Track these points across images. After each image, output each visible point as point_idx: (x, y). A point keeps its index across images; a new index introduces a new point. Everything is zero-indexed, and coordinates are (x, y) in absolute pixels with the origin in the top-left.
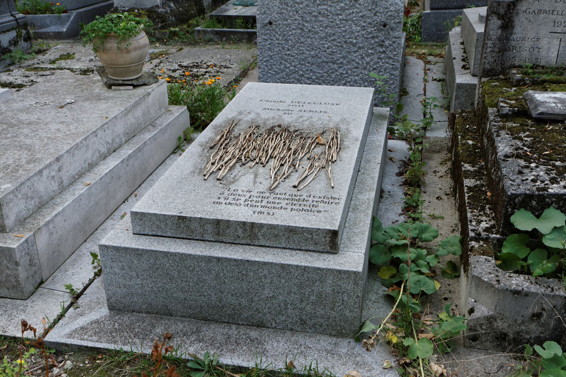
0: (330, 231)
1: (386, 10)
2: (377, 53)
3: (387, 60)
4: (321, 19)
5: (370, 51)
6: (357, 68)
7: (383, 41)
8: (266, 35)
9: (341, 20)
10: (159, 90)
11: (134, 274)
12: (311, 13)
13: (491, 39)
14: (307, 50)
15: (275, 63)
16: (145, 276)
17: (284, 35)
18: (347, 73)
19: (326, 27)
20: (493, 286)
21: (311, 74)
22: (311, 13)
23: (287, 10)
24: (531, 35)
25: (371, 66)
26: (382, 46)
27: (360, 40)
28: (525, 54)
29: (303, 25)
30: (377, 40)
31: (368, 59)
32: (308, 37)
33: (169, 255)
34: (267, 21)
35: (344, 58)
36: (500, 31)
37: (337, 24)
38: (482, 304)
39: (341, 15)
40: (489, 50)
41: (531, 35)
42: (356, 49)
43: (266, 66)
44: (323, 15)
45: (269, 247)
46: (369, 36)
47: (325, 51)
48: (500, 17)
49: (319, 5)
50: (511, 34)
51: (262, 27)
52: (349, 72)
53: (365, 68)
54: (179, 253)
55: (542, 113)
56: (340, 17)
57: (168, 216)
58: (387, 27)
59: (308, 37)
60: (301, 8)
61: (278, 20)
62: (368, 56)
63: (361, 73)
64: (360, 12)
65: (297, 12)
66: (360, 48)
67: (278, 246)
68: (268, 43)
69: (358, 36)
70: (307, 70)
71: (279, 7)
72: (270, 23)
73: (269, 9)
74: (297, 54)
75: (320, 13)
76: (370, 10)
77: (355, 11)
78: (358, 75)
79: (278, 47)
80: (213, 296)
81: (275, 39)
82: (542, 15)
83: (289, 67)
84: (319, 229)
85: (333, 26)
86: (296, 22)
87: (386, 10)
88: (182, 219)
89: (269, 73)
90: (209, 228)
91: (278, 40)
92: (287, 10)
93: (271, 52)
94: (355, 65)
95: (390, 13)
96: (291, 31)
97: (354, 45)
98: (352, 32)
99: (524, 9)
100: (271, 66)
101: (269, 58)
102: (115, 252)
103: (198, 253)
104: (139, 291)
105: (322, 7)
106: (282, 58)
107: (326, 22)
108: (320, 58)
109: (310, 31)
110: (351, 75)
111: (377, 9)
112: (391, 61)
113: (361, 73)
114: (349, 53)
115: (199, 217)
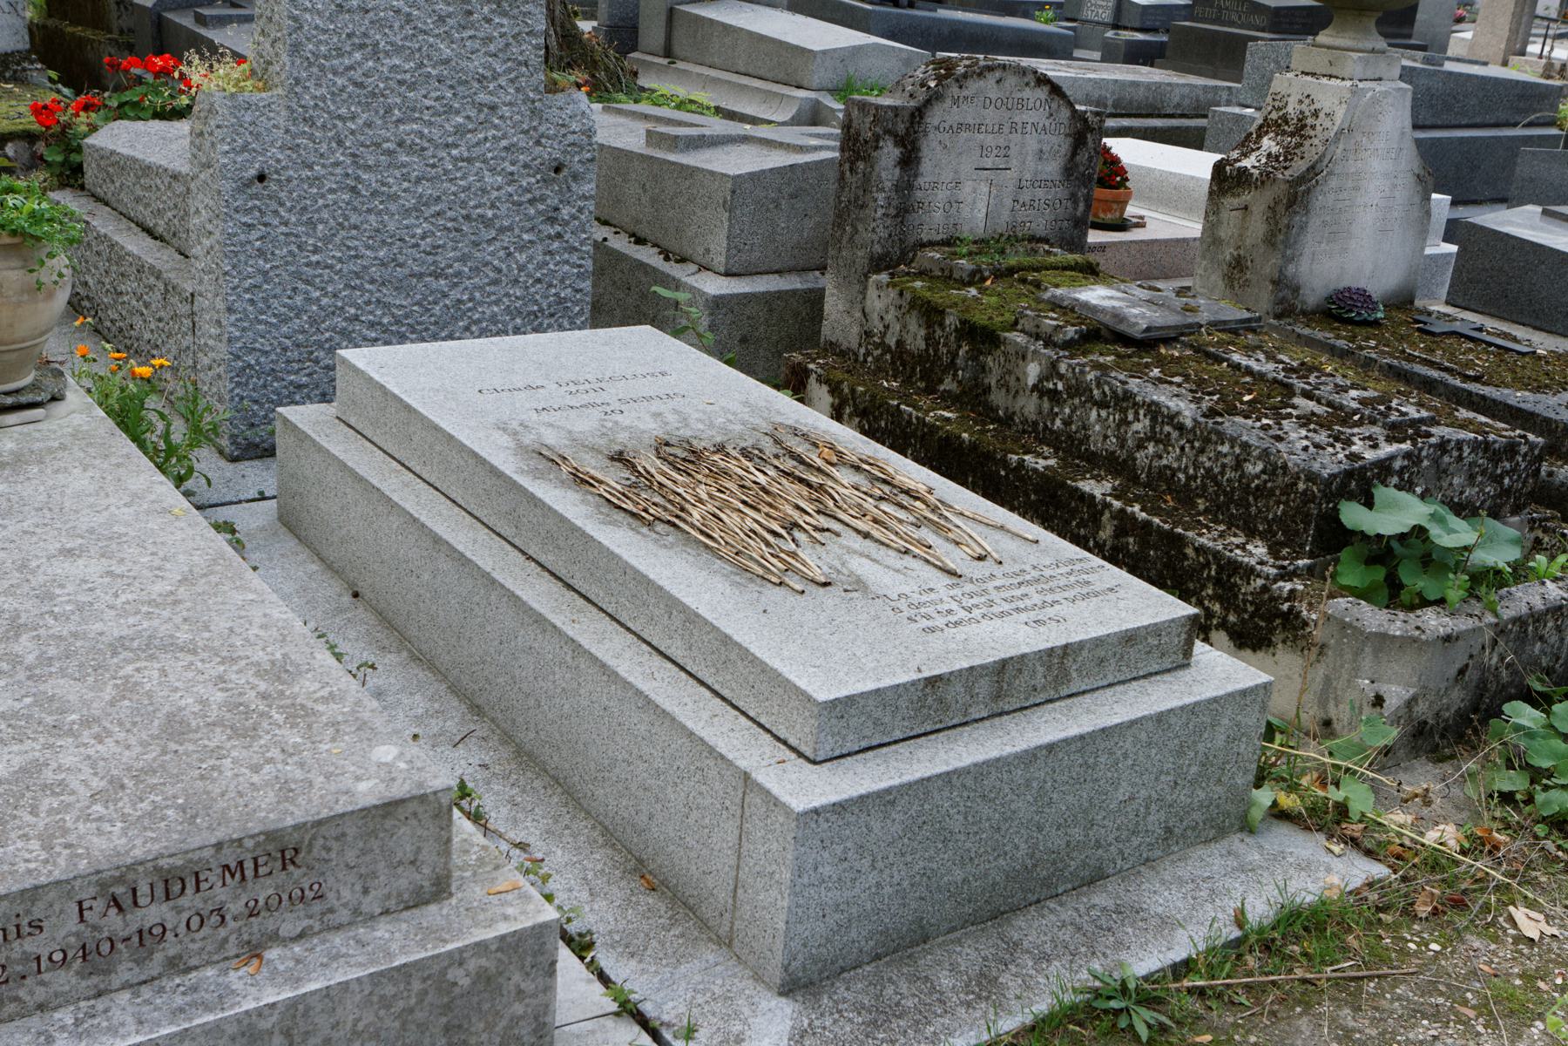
1: (563, 131)
3: (566, 256)
4: (404, 158)
5: (526, 237)
6: (495, 282)
7: (556, 209)
8: (248, 211)
9: (455, 159)
11: (866, 862)
12: (378, 145)
13: (883, 190)
14: (368, 247)
15: (278, 291)
18: (470, 300)
19: (418, 180)
20: (1415, 640)
24: (947, 176)
25: (529, 276)
26: (552, 220)
27: (504, 208)
28: (938, 215)
29: (358, 179)
30: (541, 207)
31: (522, 258)
32: (369, 211)
34: (253, 172)
35: (463, 259)
36: (897, 171)
37: (446, 172)
38: (1389, 681)
39: (457, 146)
40: (880, 212)
41: (947, 176)
42: (493, 233)
43: (252, 301)
44: (411, 149)
47: (414, 246)
48: (900, 141)
49: (399, 121)
50: (916, 176)
51: (239, 190)
52: (477, 295)
55: (1148, 329)
56: (454, 152)
58: (565, 172)
59: (369, 211)
60: (353, 132)
62: (521, 249)
64: (504, 137)
65: (340, 143)
66: (502, 230)
68: (254, 235)
69: (498, 198)
70: (368, 303)
71: (287, 131)
72: (261, 178)
73: (257, 136)
74: (340, 260)
76: (525, 132)
78: (497, 303)
79: (287, 244)
82: (964, 135)
83: (318, 299)
85: (437, 177)
86: (339, 171)
87: (563, 131)
88: (933, 682)
92: (312, 138)
93: (266, 261)
94: (492, 274)
95: (571, 138)
96: (323, 196)
97: (488, 223)
98: (484, 191)
99: (936, 123)
100: (265, 300)
101: (259, 279)
106: (297, 275)
107: (417, 166)
108: (401, 265)
109: (375, 194)
110: (481, 303)
111: (542, 129)
112: (574, 258)
113: (507, 295)
114: (476, 244)
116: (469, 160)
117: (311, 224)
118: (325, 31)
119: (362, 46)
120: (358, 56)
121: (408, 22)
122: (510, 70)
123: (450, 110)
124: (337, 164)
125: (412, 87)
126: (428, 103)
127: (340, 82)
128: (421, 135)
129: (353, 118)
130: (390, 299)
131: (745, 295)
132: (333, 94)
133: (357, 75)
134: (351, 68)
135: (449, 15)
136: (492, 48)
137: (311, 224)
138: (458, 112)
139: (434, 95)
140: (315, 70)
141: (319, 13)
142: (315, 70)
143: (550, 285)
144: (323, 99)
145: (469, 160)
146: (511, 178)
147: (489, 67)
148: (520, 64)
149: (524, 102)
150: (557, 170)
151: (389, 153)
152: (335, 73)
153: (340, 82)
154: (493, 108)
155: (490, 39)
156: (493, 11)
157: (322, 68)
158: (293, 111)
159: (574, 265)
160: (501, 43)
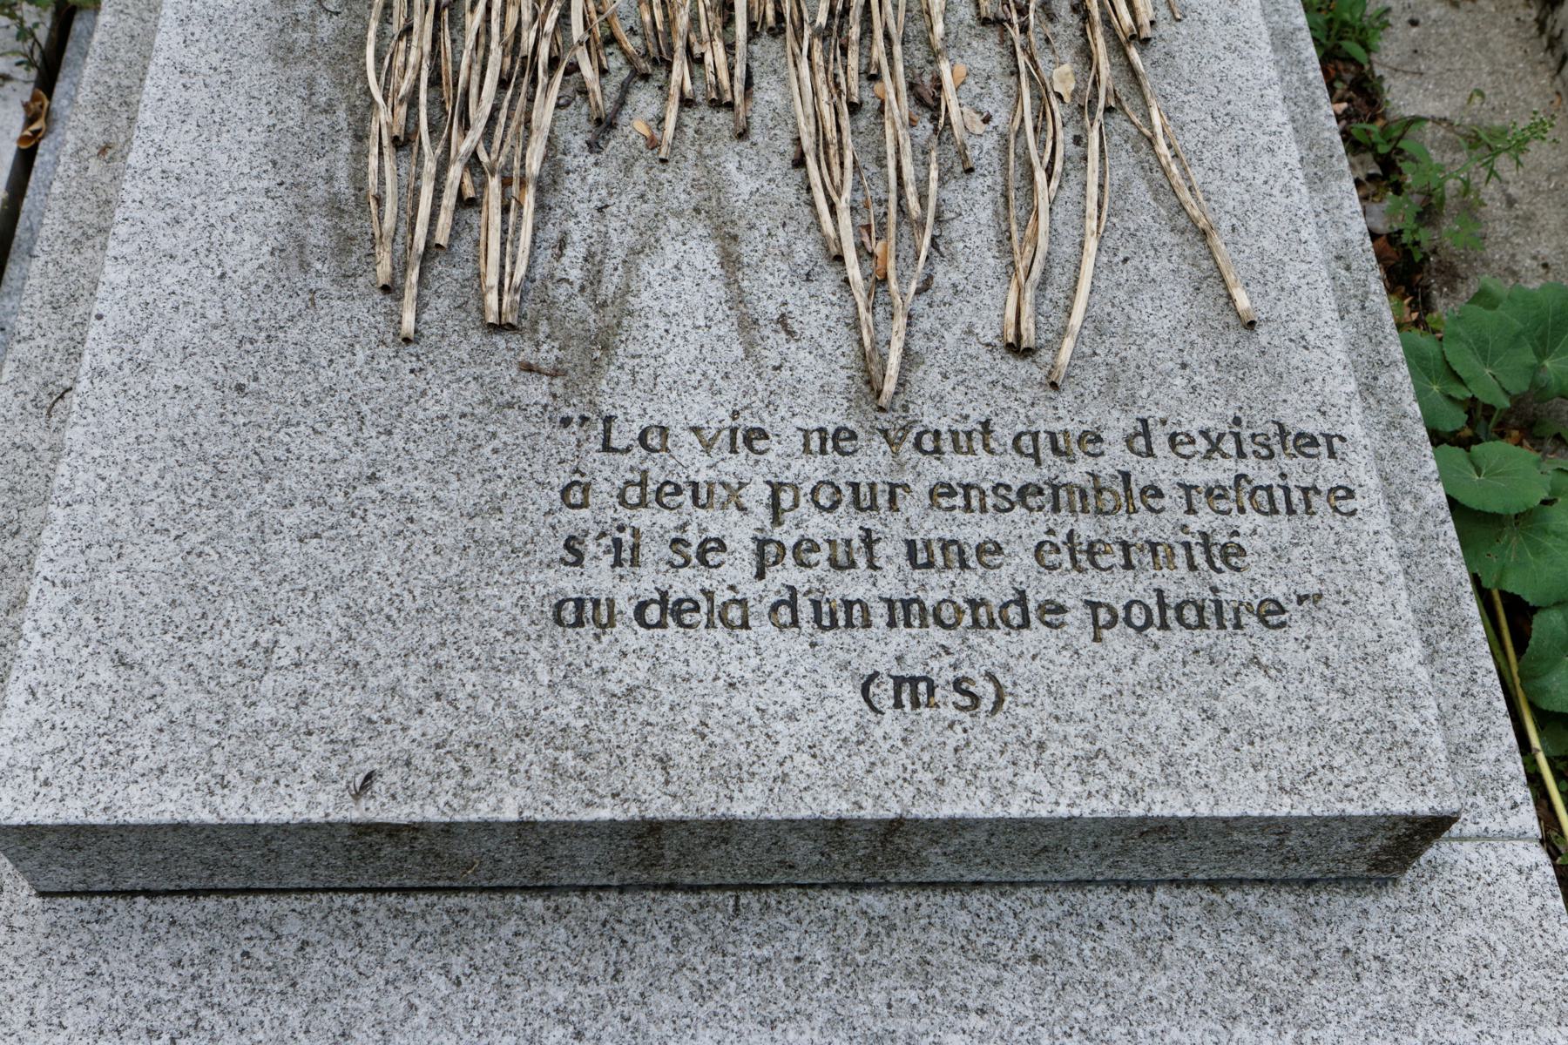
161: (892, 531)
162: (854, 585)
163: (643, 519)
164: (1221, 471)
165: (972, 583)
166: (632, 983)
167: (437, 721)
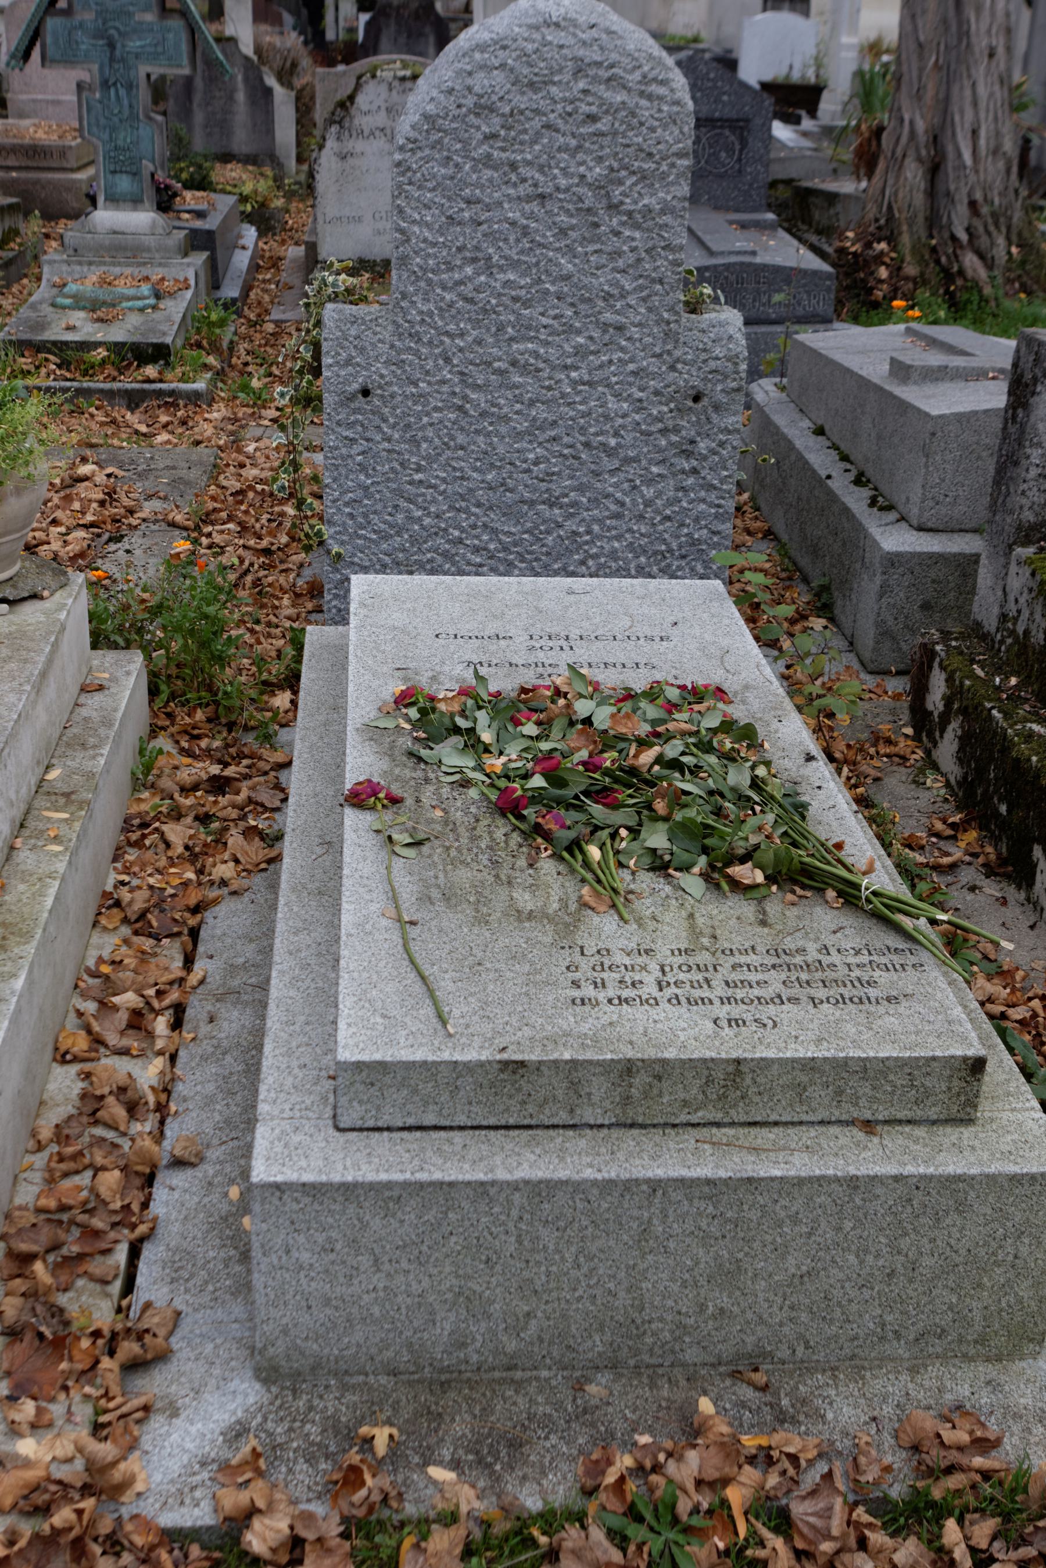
0: (965, 1059)
1: (704, 356)
2: (674, 475)
3: (703, 494)
4: (517, 379)
5: (655, 469)
6: (617, 516)
7: (692, 442)
8: (350, 425)
9: (574, 383)
10: (69, 605)
11: (365, 1261)
12: (489, 364)
14: (475, 469)
15: (379, 507)
16: (404, 1265)
17: (408, 426)
18: (588, 532)
19: (532, 403)
21: (485, 537)
22: (489, 364)
23: (417, 353)
25: (657, 512)
26: (687, 454)
29: (465, 398)
30: (674, 438)
31: (649, 492)
32: (477, 432)
33: (493, 1191)
34: (356, 386)
35: (581, 489)
37: (563, 395)
39: (577, 368)
40: (1033, 472)
42: (616, 464)
43: (351, 516)
44: (524, 369)
45: (776, 1124)
46: (653, 429)
47: (528, 471)
49: (512, 339)
51: (342, 404)
52: (596, 528)
53: (641, 517)
54: (527, 1182)
56: (574, 374)
57: (466, 1064)
58: (705, 401)
59: (477, 432)
60: (461, 350)
61: (389, 384)
62: (650, 482)
63: (630, 530)
64: (632, 360)
65: (447, 360)
66: (628, 461)
67: (805, 1118)
68: (356, 449)
69: (623, 427)
70: (474, 527)
71: (392, 346)
72: (366, 392)
73: (362, 350)
75: (514, 363)
76: (659, 356)
77: (615, 357)
78: (619, 538)
80: (622, 1294)
81: (378, 438)
83: (420, 519)
84: (934, 1058)
85: (554, 400)
86: (445, 388)
87: (704, 356)
89: (360, 537)
90: (598, 1088)
91: (389, 440)
92: (417, 353)
93: (367, 476)
94: (613, 507)
95: (713, 364)
96: (428, 414)
97: (611, 452)
98: (607, 417)
100: (365, 515)
101: (360, 493)
102: (307, 1200)
103: (589, 1173)
104: (376, 1311)
105: (522, 347)
106: (399, 493)
107: (531, 388)
108: (511, 491)
109: (483, 414)
110: (600, 537)
112: (712, 497)
113: (630, 530)
114: (596, 474)
115: (567, 1056)
116: (589, 383)
117: (415, 442)
118: (434, 244)
119: (474, 260)
120: (469, 270)
121: (525, 234)
122: (641, 288)
123: (570, 330)
124: (443, 382)
125: (527, 304)
126: (544, 321)
127: (448, 297)
128: (536, 355)
129: (462, 335)
130: (497, 525)
131: (931, 555)
132: (441, 309)
133: (467, 290)
134: (461, 283)
135: (572, 228)
136: (620, 263)
137: (415, 442)
138: (579, 332)
139: (552, 313)
140: (423, 284)
141: (428, 225)
142: (423, 284)
143: (682, 525)
144: (430, 314)
145: (589, 383)
146: (639, 406)
147: (616, 284)
148: (653, 281)
149: (657, 323)
150: (696, 399)
151: (500, 372)
152: (444, 288)
153: (448, 297)
154: (620, 328)
155: (620, 254)
156: (623, 224)
157: (430, 282)
158: (398, 326)
159: (712, 505)
160: (631, 258)
161: (717, 982)
162: (706, 993)
163: (605, 975)
164: (865, 958)
165: (757, 992)
166: (620, 1155)
167: (527, 1032)
